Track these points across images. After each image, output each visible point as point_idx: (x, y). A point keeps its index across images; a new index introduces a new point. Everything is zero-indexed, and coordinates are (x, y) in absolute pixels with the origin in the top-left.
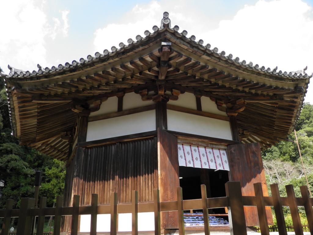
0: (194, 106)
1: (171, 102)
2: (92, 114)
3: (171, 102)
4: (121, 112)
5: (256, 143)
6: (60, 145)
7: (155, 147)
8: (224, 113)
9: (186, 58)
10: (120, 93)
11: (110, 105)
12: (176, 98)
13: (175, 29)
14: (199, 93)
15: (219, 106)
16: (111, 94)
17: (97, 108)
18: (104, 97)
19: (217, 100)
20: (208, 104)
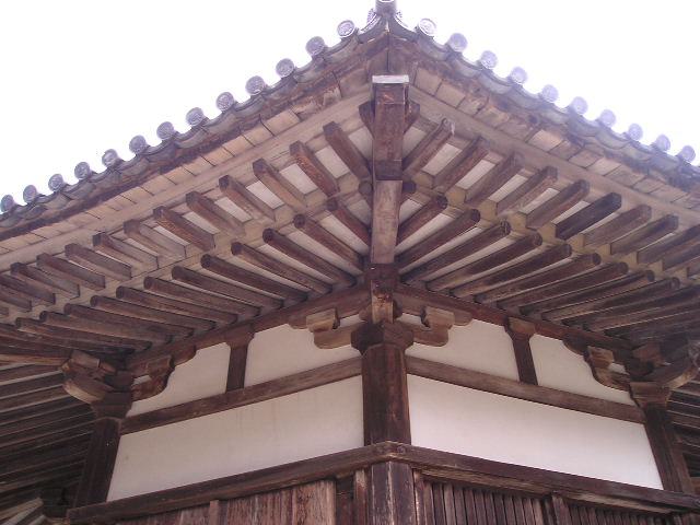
0: (507, 367)
1: (418, 350)
2: (140, 407)
3: (418, 350)
4: (237, 392)
5: (128, 404)
6: (290, 268)
7: (130, 396)
8: (621, 396)
9: (498, 159)
10: (238, 330)
11: (204, 371)
12: (439, 339)
13: (453, 46)
14: (521, 320)
15: (596, 367)
16: (212, 335)
17: (160, 382)
18: (183, 345)
19: (578, 340)
20: (557, 363)
